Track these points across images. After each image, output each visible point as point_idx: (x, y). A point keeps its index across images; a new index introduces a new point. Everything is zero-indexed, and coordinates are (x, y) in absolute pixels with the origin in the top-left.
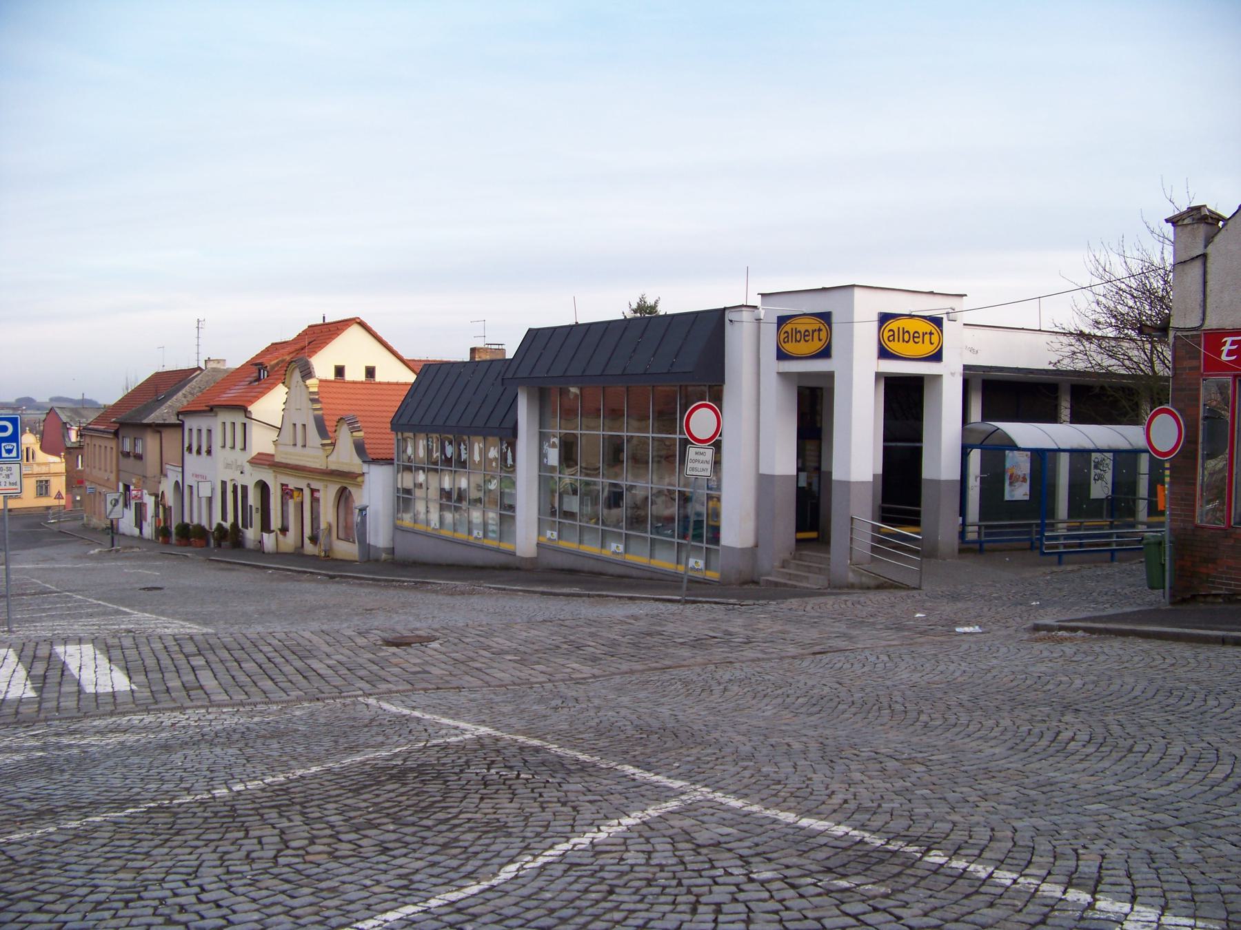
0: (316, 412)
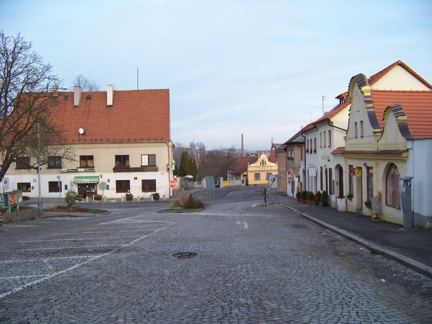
0: (369, 110)
